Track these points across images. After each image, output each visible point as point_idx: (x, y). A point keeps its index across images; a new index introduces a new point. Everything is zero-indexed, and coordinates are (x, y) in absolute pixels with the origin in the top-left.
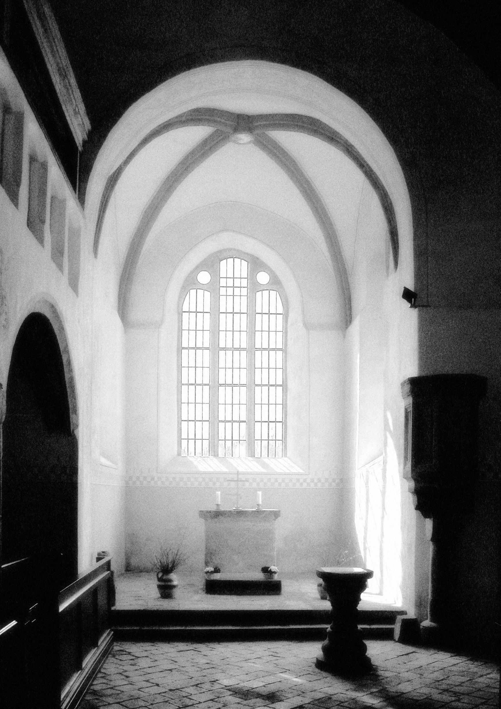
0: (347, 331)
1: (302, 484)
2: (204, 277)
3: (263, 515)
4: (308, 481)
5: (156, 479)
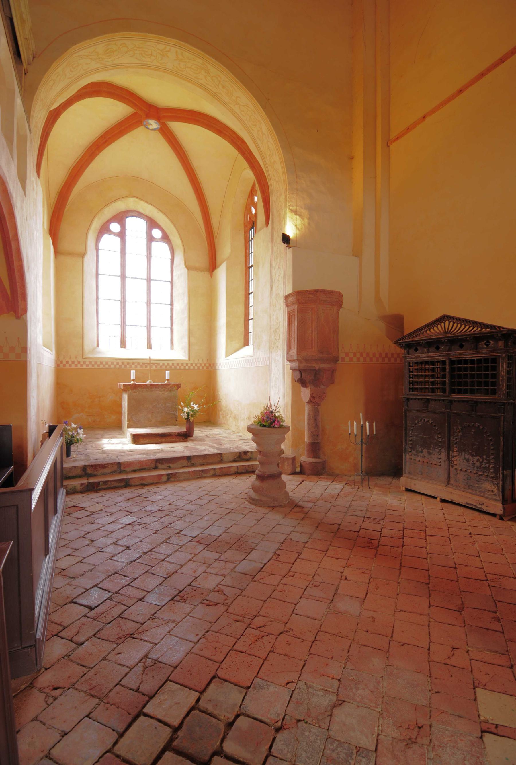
0: (214, 273)
1: (185, 367)
2: (115, 227)
3: (169, 387)
4: (189, 365)
5: (82, 363)
